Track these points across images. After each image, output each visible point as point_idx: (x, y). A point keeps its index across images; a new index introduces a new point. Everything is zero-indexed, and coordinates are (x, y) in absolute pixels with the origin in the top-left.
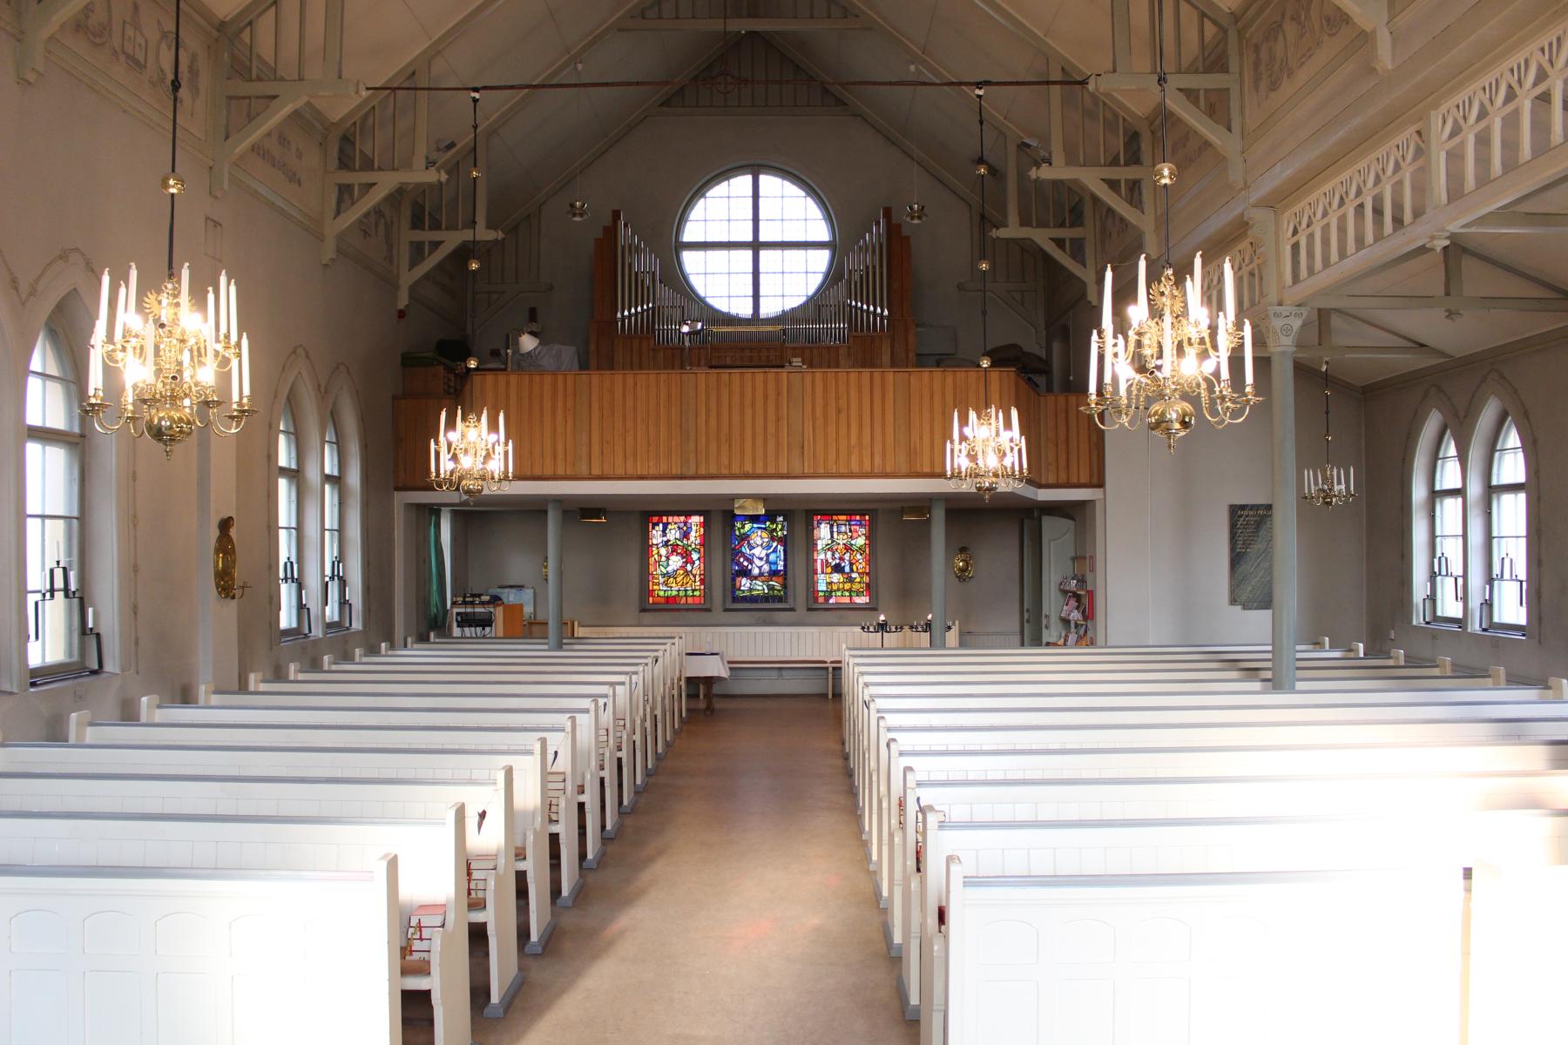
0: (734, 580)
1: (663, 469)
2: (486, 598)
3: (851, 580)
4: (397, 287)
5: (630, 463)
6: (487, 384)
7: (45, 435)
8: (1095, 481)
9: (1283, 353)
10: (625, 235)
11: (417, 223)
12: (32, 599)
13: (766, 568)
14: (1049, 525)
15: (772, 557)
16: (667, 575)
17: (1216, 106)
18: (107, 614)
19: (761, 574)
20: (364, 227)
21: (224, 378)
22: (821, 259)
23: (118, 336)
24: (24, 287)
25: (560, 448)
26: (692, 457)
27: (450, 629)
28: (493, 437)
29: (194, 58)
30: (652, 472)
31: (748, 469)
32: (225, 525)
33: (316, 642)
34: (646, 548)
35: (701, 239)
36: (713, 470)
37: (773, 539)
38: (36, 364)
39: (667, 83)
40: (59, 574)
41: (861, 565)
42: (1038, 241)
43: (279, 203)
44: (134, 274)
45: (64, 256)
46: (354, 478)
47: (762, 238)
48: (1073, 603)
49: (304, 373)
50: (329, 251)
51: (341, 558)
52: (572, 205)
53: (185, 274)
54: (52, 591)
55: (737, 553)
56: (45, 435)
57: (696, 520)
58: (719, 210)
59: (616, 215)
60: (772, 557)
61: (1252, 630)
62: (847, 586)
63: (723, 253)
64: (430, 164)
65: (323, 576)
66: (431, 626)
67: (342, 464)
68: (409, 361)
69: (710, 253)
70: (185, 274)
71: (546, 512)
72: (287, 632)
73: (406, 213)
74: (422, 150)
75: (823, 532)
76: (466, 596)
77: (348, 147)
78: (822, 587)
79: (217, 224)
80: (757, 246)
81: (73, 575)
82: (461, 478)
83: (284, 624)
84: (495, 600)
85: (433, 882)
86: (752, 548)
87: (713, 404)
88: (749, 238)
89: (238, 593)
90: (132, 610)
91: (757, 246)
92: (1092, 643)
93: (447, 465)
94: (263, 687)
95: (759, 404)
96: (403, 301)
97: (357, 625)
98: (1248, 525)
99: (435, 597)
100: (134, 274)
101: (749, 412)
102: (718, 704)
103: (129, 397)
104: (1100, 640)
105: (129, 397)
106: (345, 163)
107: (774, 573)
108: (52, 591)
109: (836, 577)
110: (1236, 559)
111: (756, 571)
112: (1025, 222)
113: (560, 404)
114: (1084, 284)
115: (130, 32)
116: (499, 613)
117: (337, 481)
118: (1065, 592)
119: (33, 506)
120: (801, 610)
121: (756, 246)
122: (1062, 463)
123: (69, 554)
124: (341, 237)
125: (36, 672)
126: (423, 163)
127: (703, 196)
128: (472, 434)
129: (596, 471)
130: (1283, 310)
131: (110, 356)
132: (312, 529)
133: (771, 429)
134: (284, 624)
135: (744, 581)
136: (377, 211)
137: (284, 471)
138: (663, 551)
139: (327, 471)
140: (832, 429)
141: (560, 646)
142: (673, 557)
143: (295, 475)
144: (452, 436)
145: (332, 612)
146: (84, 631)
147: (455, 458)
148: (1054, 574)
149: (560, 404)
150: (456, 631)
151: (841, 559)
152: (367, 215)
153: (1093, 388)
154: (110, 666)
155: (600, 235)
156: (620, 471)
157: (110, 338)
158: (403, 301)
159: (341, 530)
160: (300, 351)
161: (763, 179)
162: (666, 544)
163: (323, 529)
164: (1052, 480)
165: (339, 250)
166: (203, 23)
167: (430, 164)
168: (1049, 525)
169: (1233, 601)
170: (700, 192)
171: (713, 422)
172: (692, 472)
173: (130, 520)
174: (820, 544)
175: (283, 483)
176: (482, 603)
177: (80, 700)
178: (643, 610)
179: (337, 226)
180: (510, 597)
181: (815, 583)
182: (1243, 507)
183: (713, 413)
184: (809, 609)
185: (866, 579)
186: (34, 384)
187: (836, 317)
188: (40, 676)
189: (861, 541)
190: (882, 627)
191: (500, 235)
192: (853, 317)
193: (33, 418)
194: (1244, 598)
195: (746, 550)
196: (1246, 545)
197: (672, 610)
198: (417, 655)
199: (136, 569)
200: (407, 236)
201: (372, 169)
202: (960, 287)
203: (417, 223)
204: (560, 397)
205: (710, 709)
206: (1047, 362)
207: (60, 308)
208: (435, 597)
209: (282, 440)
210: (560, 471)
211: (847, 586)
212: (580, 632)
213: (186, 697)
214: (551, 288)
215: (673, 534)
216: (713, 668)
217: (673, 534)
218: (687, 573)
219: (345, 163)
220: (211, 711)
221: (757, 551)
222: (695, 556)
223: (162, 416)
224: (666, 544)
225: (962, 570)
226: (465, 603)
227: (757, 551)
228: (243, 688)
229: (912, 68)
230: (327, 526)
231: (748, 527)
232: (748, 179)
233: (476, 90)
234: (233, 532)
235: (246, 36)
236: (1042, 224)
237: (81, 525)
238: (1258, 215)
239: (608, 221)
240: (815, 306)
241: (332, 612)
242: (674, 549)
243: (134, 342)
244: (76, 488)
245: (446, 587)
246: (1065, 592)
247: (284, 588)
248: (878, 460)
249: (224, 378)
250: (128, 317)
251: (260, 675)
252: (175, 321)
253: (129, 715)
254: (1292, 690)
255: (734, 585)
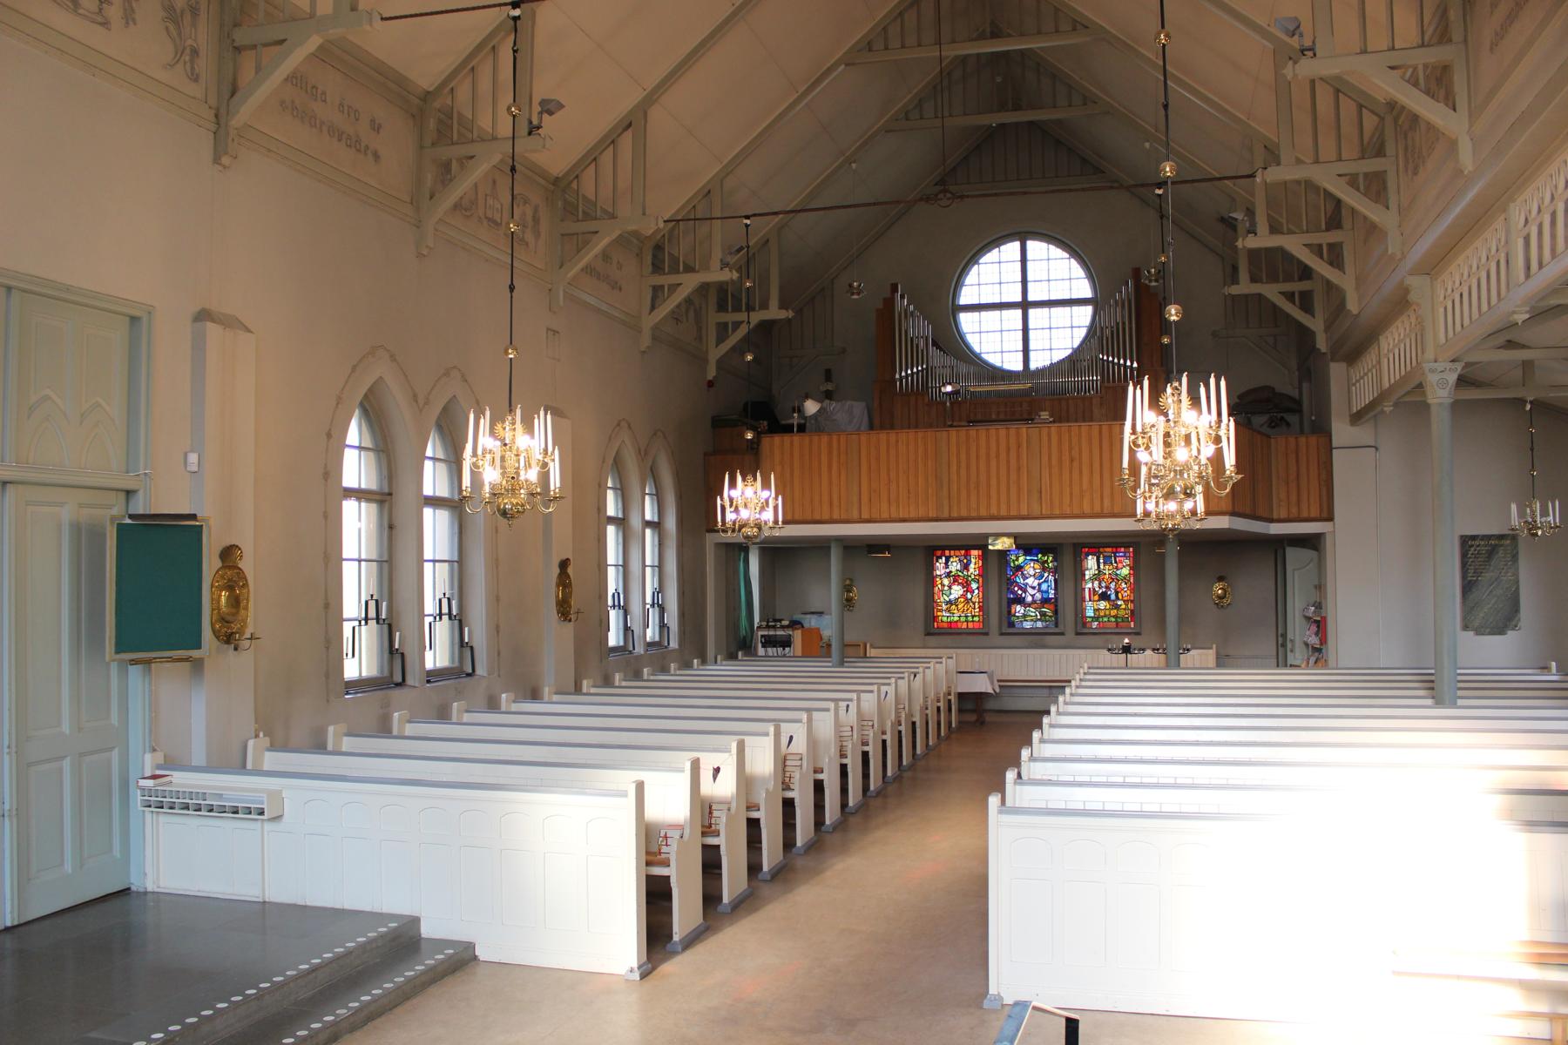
0: (1009, 607)
1: (921, 513)
2: (785, 623)
3: (1117, 607)
4: (706, 361)
5: (893, 509)
6: (775, 444)
7: (435, 502)
8: (1325, 515)
9: (1440, 404)
10: (902, 303)
11: (722, 307)
12: (428, 620)
13: (1038, 596)
14: (1292, 554)
15: (1044, 587)
16: (950, 603)
17: (1375, 186)
18: (477, 632)
19: (1034, 602)
20: (675, 316)
21: (544, 477)
22: (1084, 315)
23: (480, 452)
24: (421, 402)
25: (835, 497)
26: (946, 502)
27: (756, 649)
28: (766, 494)
29: (536, 210)
30: (912, 515)
31: (994, 511)
32: (564, 565)
33: (639, 657)
34: (931, 580)
35: (976, 302)
36: (964, 513)
37: (1044, 569)
38: (429, 453)
39: (898, 202)
40: (445, 602)
41: (1126, 593)
42: (1269, 296)
43: (604, 307)
44: (488, 413)
45: (447, 374)
46: (671, 523)
47: (1031, 298)
48: (1314, 628)
49: (628, 442)
50: (646, 340)
51: (660, 590)
52: (851, 286)
53: (518, 412)
54: (441, 615)
55: (1011, 583)
56: (435, 502)
57: (975, 553)
58: (991, 274)
59: (894, 288)
60: (1044, 587)
61: (1493, 652)
62: (1114, 612)
63: (995, 314)
64: (724, 265)
65: (644, 603)
66: (740, 646)
67: (661, 511)
68: (718, 423)
69: (984, 314)
70: (518, 412)
71: (829, 548)
72: (614, 649)
73: (713, 299)
74: (717, 254)
75: (1091, 562)
76: (770, 620)
77: (660, 255)
78: (1090, 613)
79: (555, 332)
80: (1025, 303)
81: (454, 603)
82: (741, 527)
83: (612, 642)
84: (795, 624)
85: (670, 802)
86: (1025, 578)
87: (963, 457)
88: (1018, 298)
89: (573, 617)
90: (496, 630)
91: (1025, 303)
92: (1326, 666)
93: (730, 516)
94: (593, 690)
95: (1003, 455)
96: (711, 373)
97: (674, 644)
98: (1481, 554)
99: (744, 622)
100: (488, 413)
101: (993, 463)
102: (988, 718)
103: (487, 488)
104: (1331, 662)
105: (487, 488)
106: (657, 268)
107: (1045, 601)
108: (441, 615)
109: (1103, 604)
110: (1467, 587)
111: (1029, 599)
112: (1254, 279)
113: (835, 459)
114: (1313, 333)
115: (490, 201)
116: (797, 636)
117: (656, 526)
118: (1308, 618)
119: (428, 555)
120: (1070, 634)
121: (1025, 305)
122: (1294, 498)
123: (452, 588)
124: (655, 328)
125: (430, 673)
126: (718, 265)
127: (977, 262)
128: (749, 492)
129: (865, 516)
130: (1440, 366)
131: (475, 465)
132: (635, 566)
133: (1013, 476)
134: (612, 642)
135: (1018, 608)
136: (688, 301)
137: (611, 520)
138: (946, 582)
139: (648, 517)
140: (1066, 476)
141: (842, 664)
142: (955, 591)
143: (621, 522)
144: (734, 493)
145: (651, 634)
146: (462, 644)
147: (736, 510)
148: (1297, 603)
149: (835, 459)
150: (761, 651)
151: (1108, 588)
152: (678, 306)
153: (1125, 464)
154: (480, 671)
155: (881, 306)
156: (885, 515)
157: (475, 454)
158: (711, 373)
159: (660, 567)
160: (623, 424)
161: (1031, 244)
162: (948, 575)
163: (644, 566)
164: (1283, 515)
165: (654, 338)
166: (543, 182)
167: (724, 265)
168: (1292, 554)
169: (1466, 627)
170: (974, 259)
171: (963, 472)
172: (946, 515)
173: (494, 563)
174: (1088, 575)
175: (611, 530)
176: (783, 627)
177: (459, 694)
178: (928, 634)
179: (649, 321)
180: (811, 622)
181: (1083, 610)
182: (1474, 538)
183: (964, 464)
184: (1077, 634)
185: (1130, 606)
186: (428, 465)
187: (1090, 371)
188: (433, 676)
189: (1125, 571)
190: (1127, 650)
191: (790, 314)
192: (1104, 368)
193: (428, 490)
194: (1476, 624)
195: (1020, 580)
196: (1478, 573)
197: (952, 635)
198: (726, 669)
199: (498, 599)
200: (714, 318)
201: (678, 272)
202: (1214, 334)
203: (722, 307)
204: (835, 453)
205: (981, 723)
206: (1299, 403)
207: (445, 409)
208: (744, 622)
209: (610, 495)
210: (836, 516)
211: (1114, 612)
212: (871, 652)
213: (535, 695)
214: (844, 351)
215: (955, 566)
216: (981, 685)
217: (955, 566)
218: (967, 601)
219: (657, 268)
220: (552, 705)
221: (1030, 581)
222: (974, 586)
223: (507, 503)
224: (948, 575)
225: (1220, 597)
226: (768, 627)
227: (1030, 581)
228: (578, 690)
229: (1147, 145)
230: (648, 562)
231: (1021, 559)
232: (1017, 245)
233: (747, 217)
234: (570, 570)
235: (574, 185)
236: (1273, 278)
237: (459, 566)
238: (1415, 282)
239: (888, 295)
240: (1073, 362)
241: (651, 634)
242: (956, 579)
243: (488, 456)
244: (456, 530)
245: (741, 616)
246: (1308, 618)
247: (613, 614)
248: (1107, 502)
249: (544, 477)
250: (486, 441)
251: (591, 682)
252: (513, 440)
253: (493, 705)
254: (1454, 705)
255: (1009, 612)
